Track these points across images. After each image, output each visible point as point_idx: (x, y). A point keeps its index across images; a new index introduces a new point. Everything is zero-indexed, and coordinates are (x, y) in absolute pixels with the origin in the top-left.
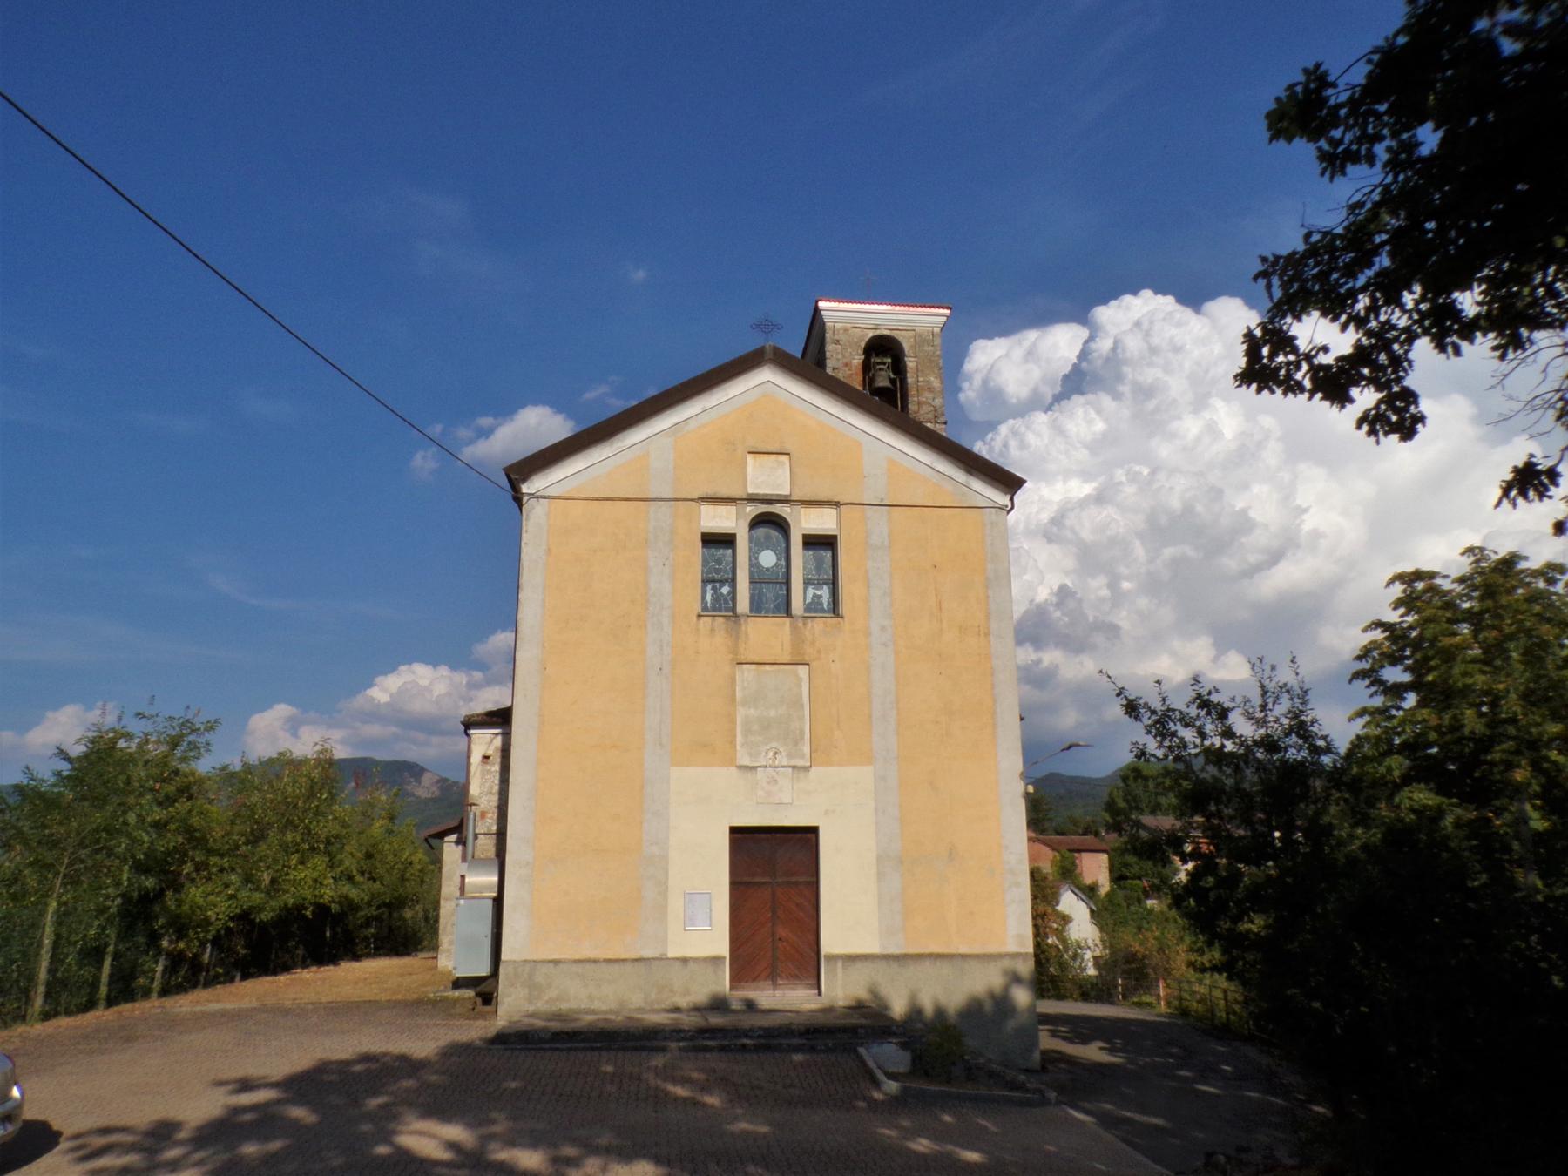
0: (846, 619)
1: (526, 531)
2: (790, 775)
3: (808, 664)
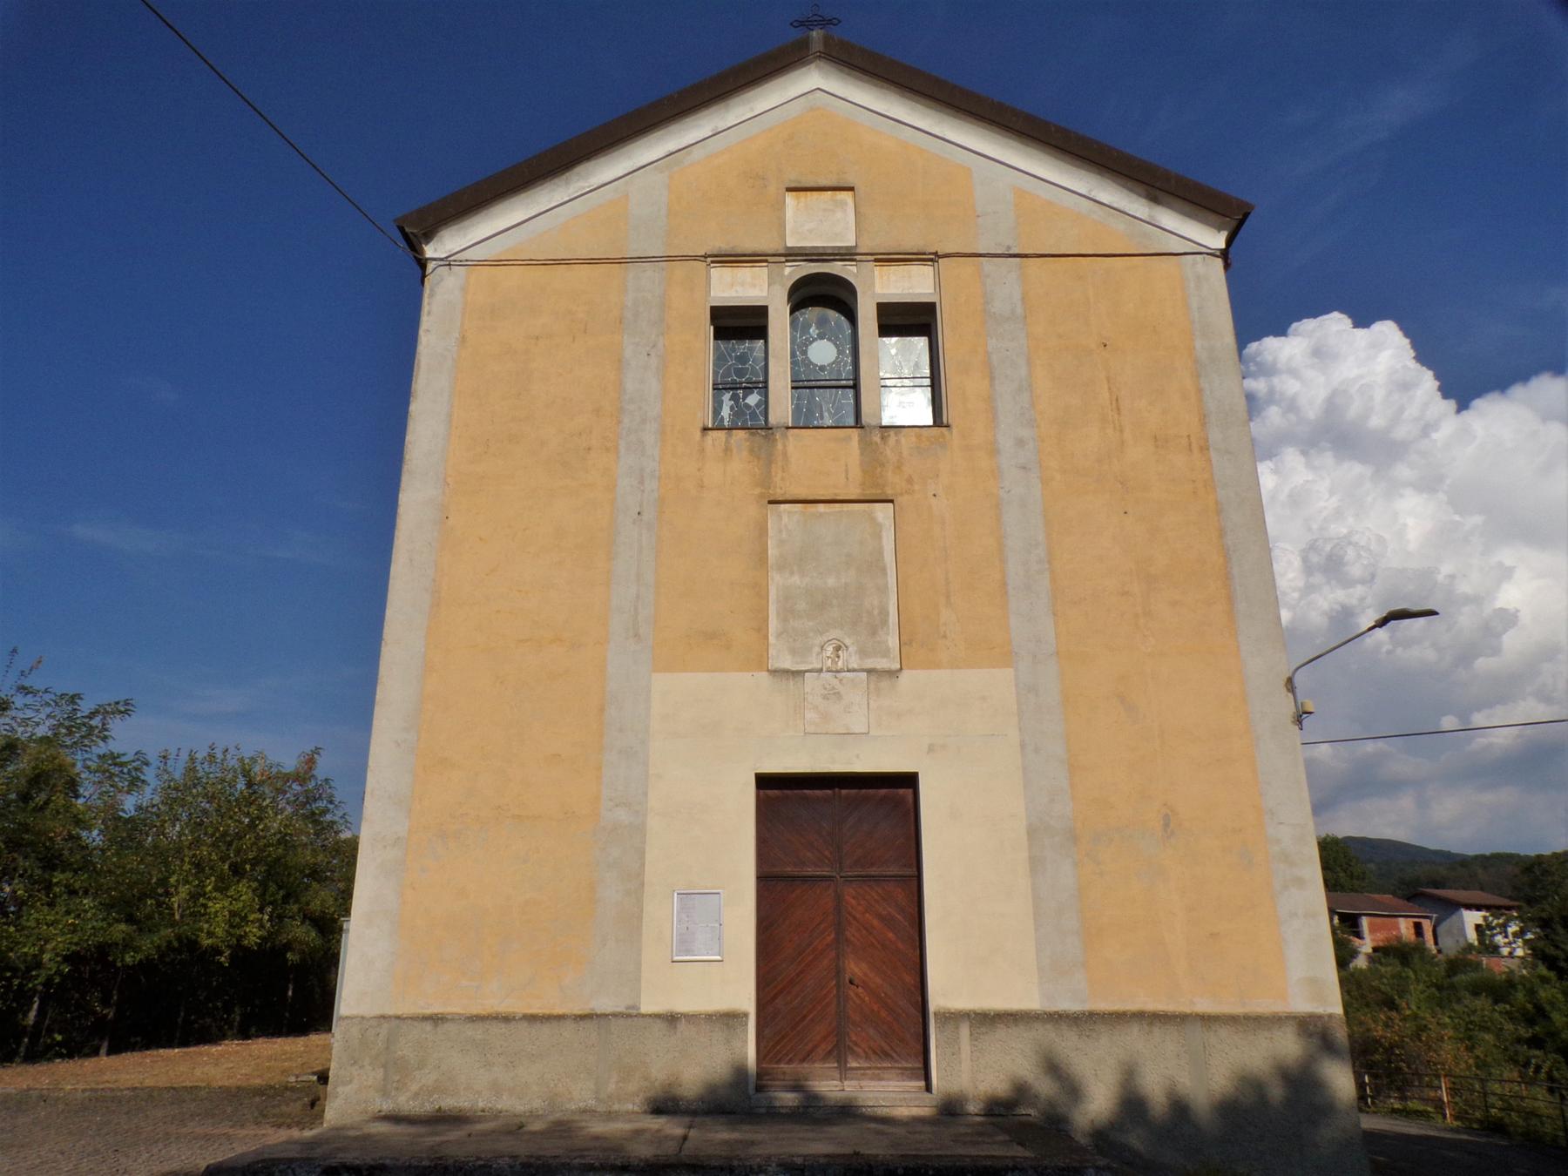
0: (955, 430)
1: (429, 313)
3: (892, 501)
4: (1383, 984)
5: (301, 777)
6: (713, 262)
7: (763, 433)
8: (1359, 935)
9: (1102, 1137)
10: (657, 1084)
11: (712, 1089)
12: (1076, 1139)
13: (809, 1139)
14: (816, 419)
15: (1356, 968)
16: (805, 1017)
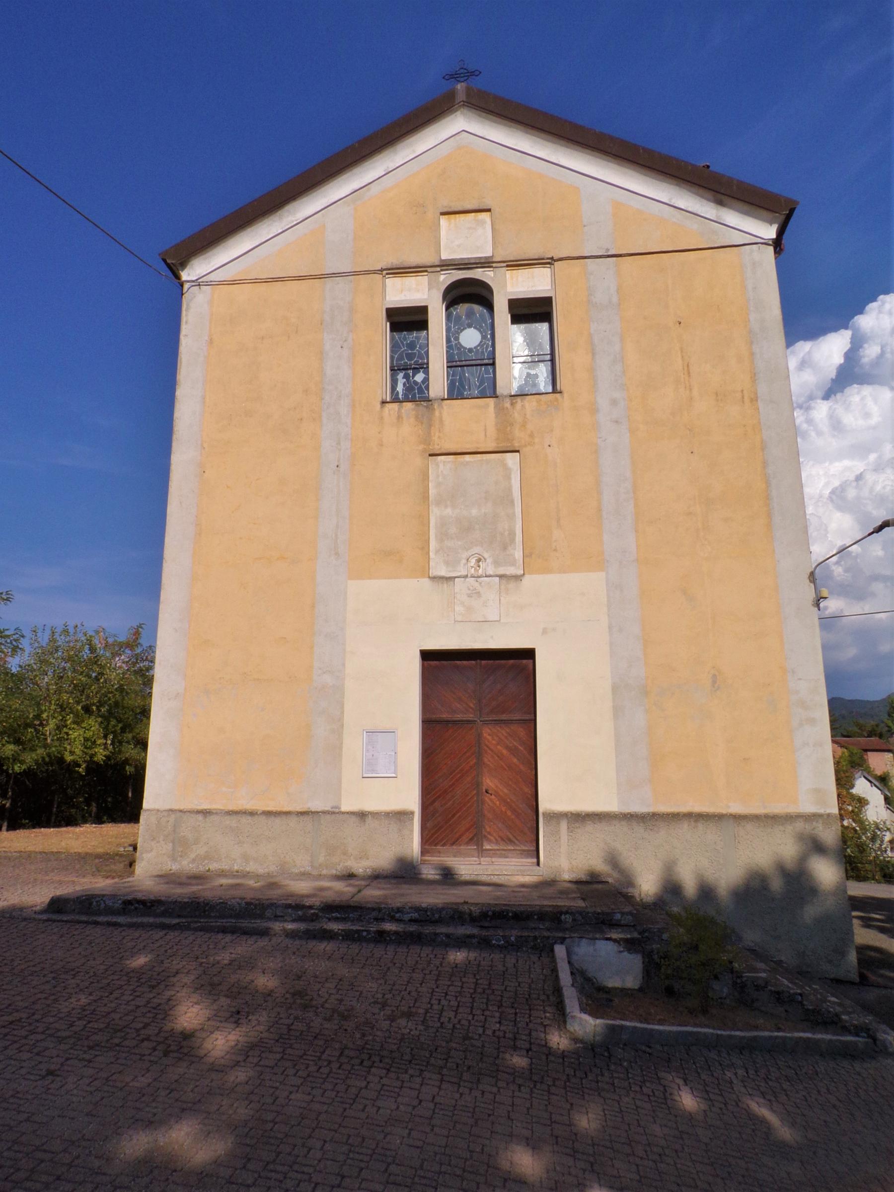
0: (565, 395)
1: (186, 322)
2: (497, 586)
3: (518, 451)
7: (424, 404)
16: (454, 815)
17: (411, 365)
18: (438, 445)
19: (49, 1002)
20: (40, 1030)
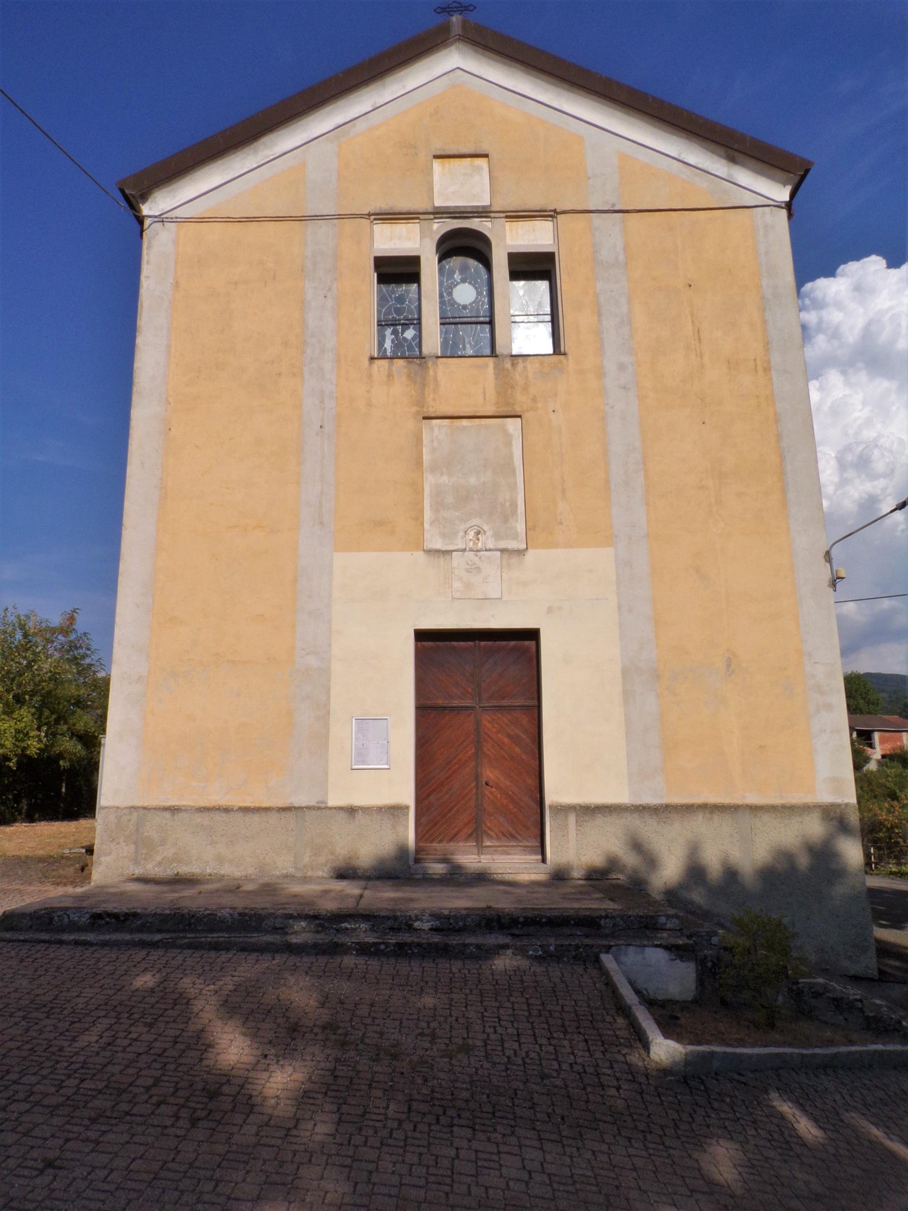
0: (570, 357)
1: (148, 262)
3: (520, 416)
4: (889, 782)
5: (65, 630)
6: (375, 219)
7: (418, 361)
8: (871, 746)
9: (672, 895)
10: (340, 857)
11: (381, 861)
12: (653, 896)
13: (453, 897)
14: (460, 350)
15: (868, 771)
16: (450, 811)
17: (399, 320)
18: (433, 407)
19: (25, 1053)
20: (21, 1096)
